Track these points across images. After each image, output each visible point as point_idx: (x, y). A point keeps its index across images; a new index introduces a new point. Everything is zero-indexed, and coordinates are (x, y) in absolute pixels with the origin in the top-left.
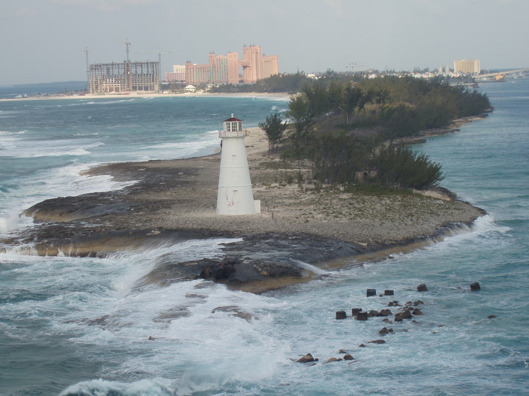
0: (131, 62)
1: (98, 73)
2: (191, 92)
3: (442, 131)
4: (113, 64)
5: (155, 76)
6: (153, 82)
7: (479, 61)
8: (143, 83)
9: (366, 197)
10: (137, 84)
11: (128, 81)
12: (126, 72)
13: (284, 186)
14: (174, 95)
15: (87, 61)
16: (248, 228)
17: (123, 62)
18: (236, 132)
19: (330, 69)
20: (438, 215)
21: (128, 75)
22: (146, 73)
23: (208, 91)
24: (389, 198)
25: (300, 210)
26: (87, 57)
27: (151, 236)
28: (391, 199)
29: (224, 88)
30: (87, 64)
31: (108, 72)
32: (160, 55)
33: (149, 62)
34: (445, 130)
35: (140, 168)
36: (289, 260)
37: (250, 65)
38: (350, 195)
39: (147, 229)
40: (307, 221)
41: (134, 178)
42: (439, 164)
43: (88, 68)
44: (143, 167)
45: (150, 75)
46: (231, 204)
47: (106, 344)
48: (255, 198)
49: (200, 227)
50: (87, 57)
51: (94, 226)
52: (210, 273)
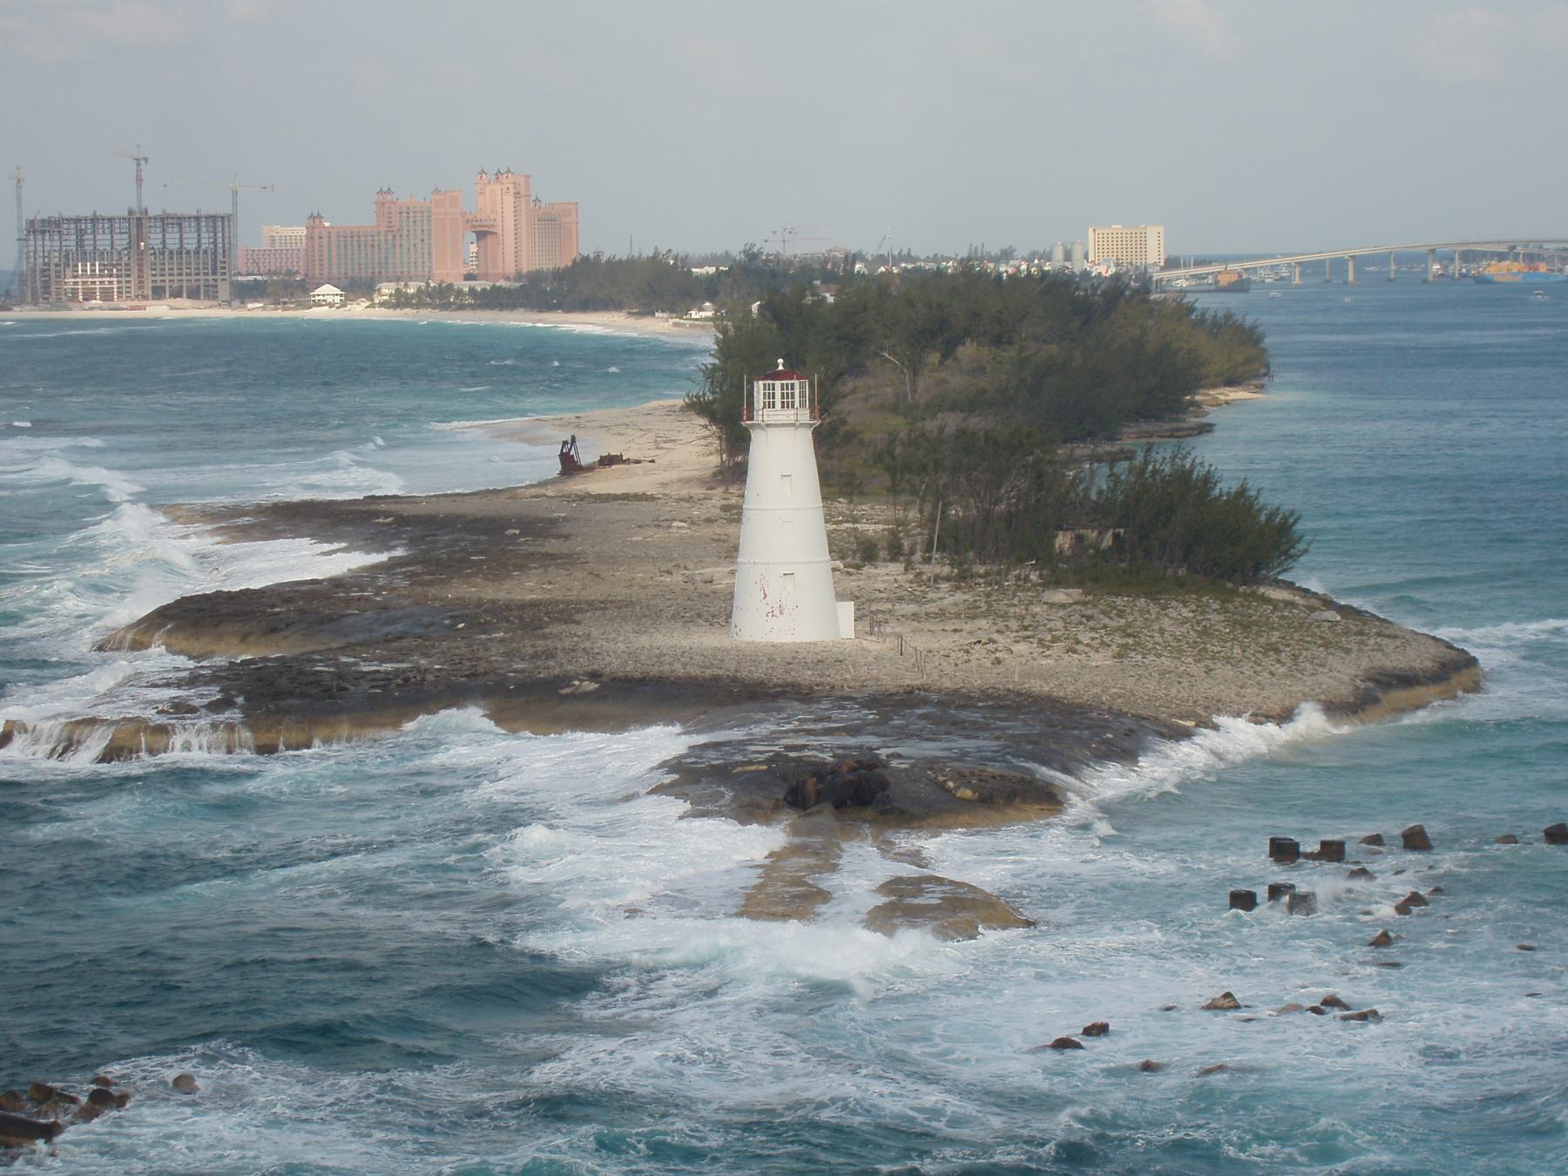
0: (151, 214)
1: (51, 243)
2: (331, 305)
3: (1167, 426)
4: (95, 220)
5: (220, 257)
6: (214, 273)
7: (1161, 229)
8: (184, 278)
9: (1119, 601)
10: (167, 278)
11: (141, 271)
12: (134, 243)
13: (858, 567)
14: (279, 313)
15: (19, 207)
16: (848, 676)
17: (126, 214)
18: (792, 412)
19: (753, 245)
20: (1348, 651)
21: (141, 253)
22: (192, 247)
23: (382, 304)
24: (1184, 603)
25: (955, 631)
26: (19, 198)
27: (573, 696)
28: (1193, 607)
29: (430, 296)
30: (20, 218)
31: (80, 243)
32: (235, 193)
33: (203, 213)
34: (1175, 425)
35: (377, 514)
36: (1005, 761)
37: (499, 231)
38: (1076, 593)
39: (556, 676)
40: (998, 661)
41: (371, 544)
42: (1292, 513)
43: (20, 230)
44: (387, 514)
45: (205, 252)
46: (777, 613)
47: (205, 1078)
48: (841, 596)
49: (708, 672)
50: (19, 198)
51: (388, 667)
52: (819, 793)
